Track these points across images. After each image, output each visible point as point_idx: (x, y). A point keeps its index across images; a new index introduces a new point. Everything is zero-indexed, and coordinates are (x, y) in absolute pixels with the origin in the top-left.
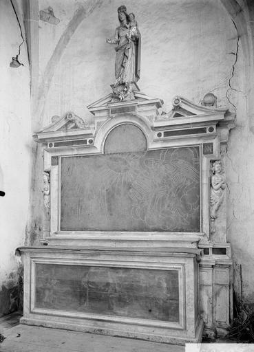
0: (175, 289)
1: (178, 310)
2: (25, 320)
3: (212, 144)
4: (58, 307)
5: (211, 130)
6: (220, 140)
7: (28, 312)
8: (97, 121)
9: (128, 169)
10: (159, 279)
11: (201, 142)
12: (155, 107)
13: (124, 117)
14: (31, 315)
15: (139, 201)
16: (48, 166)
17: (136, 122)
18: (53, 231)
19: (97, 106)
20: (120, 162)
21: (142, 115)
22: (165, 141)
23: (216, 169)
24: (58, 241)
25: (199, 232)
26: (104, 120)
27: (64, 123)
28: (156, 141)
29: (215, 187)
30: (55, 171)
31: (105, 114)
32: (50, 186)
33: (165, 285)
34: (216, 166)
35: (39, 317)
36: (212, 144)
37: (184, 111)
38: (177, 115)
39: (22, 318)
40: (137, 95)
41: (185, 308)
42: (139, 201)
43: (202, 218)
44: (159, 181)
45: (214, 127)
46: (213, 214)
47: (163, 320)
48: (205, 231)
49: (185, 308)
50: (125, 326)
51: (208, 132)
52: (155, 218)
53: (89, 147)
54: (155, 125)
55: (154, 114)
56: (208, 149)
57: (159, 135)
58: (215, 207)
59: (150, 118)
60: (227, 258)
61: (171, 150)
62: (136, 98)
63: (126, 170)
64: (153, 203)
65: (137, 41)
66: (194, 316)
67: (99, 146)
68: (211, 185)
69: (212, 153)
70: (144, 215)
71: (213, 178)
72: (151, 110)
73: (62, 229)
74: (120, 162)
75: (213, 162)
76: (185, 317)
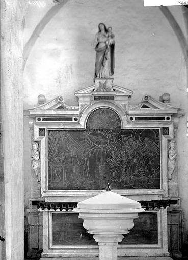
0: (155, 224)
1: (157, 237)
2: (46, 255)
3: (168, 128)
4: (72, 243)
5: (168, 119)
6: (174, 126)
7: (47, 249)
8: (80, 104)
9: (106, 143)
10: (145, 218)
11: (161, 126)
12: (127, 98)
13: (103, 103)
14: (49, 250)
15: (116, 167)
16: (36, 136)
17: (113, 108)
18: (43, 190)
19: (82, 92)
20: (99, 136)
21: (116, 103)
22: (135, 123)
23: (172, 146)
24: (55, 198)
25: (160, 189)
26: (87, 103)
27: (54, 103)
28: (129, 123)
29: (171, 158)
30: (44, 141)
31: (87, 99)
32: (40, 153)
33: (149, 222)
34: (172, 144)
35: (57, 251)
36: (168, 128)
37: (150, 104)
38: (144, 107)
39: (43, 254)
40: (115, 88)
41: (162, 235)
42: (116, 167)
43: (162, 180)
44: (131, 152)
45: (170, 117)
46: (170, 177)
47: (147, 244)
48: (164, 188)
49: (162, 235)
50: (123, 250)
51: (166, 120)
52: (79, 181)
53: (74, 124)
54: (130, 112)
55: (127, 103)
56: (165, 131)
57: (132, 119)
58: (171, 172)
59: (125, 106)
60: (159, 252)
61: (139, 131)
62: (114, 90)
63: (104, 143)
64: (126, 169)
65: (112, 46)
66: (167, 239)
67: (82, 125)
68: (168, 157)
69: (168, 134)
70: (119, 178)
71: (170, 152)
72: (124, 100)
73: (49, 189)
74: (99, 136)
75: (169, 141)
76: (162, 240)
